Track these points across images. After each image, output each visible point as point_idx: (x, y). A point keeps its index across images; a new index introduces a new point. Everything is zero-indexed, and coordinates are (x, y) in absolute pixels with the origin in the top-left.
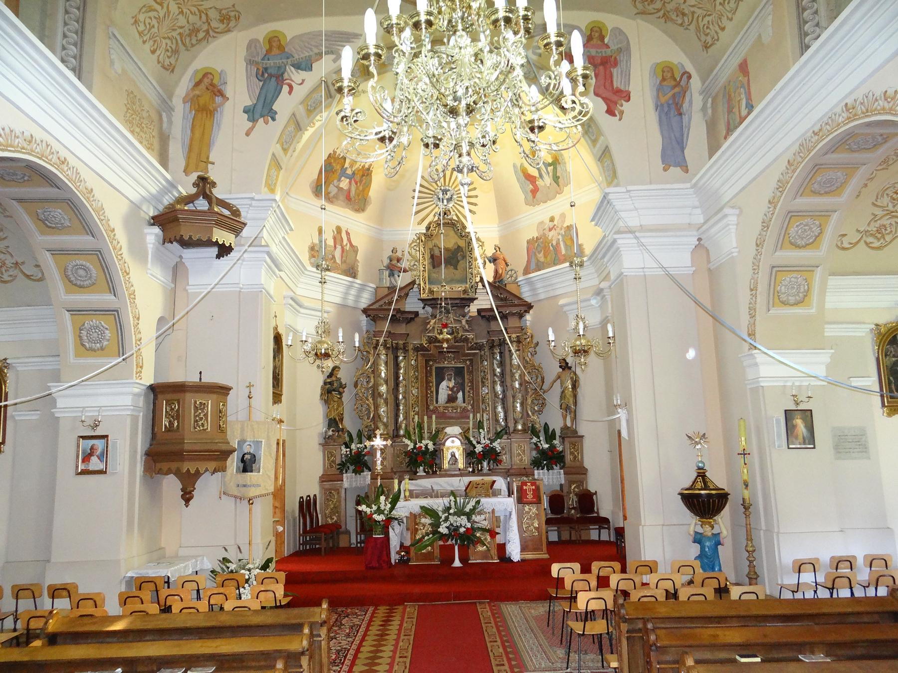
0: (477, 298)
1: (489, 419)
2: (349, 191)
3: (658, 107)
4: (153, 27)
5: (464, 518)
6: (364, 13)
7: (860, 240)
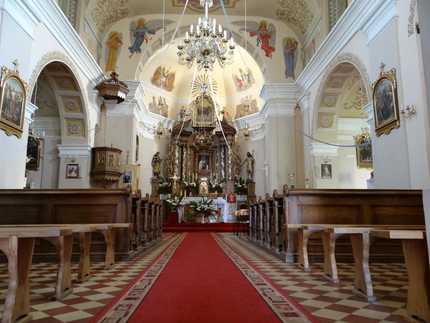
0: (215, 128)
1: (218, 176)
2: (165, 83)
3: (285, 54)
4: (98, 16)
5: (207, 205)
6: (185, 33)
7: (352, 106)
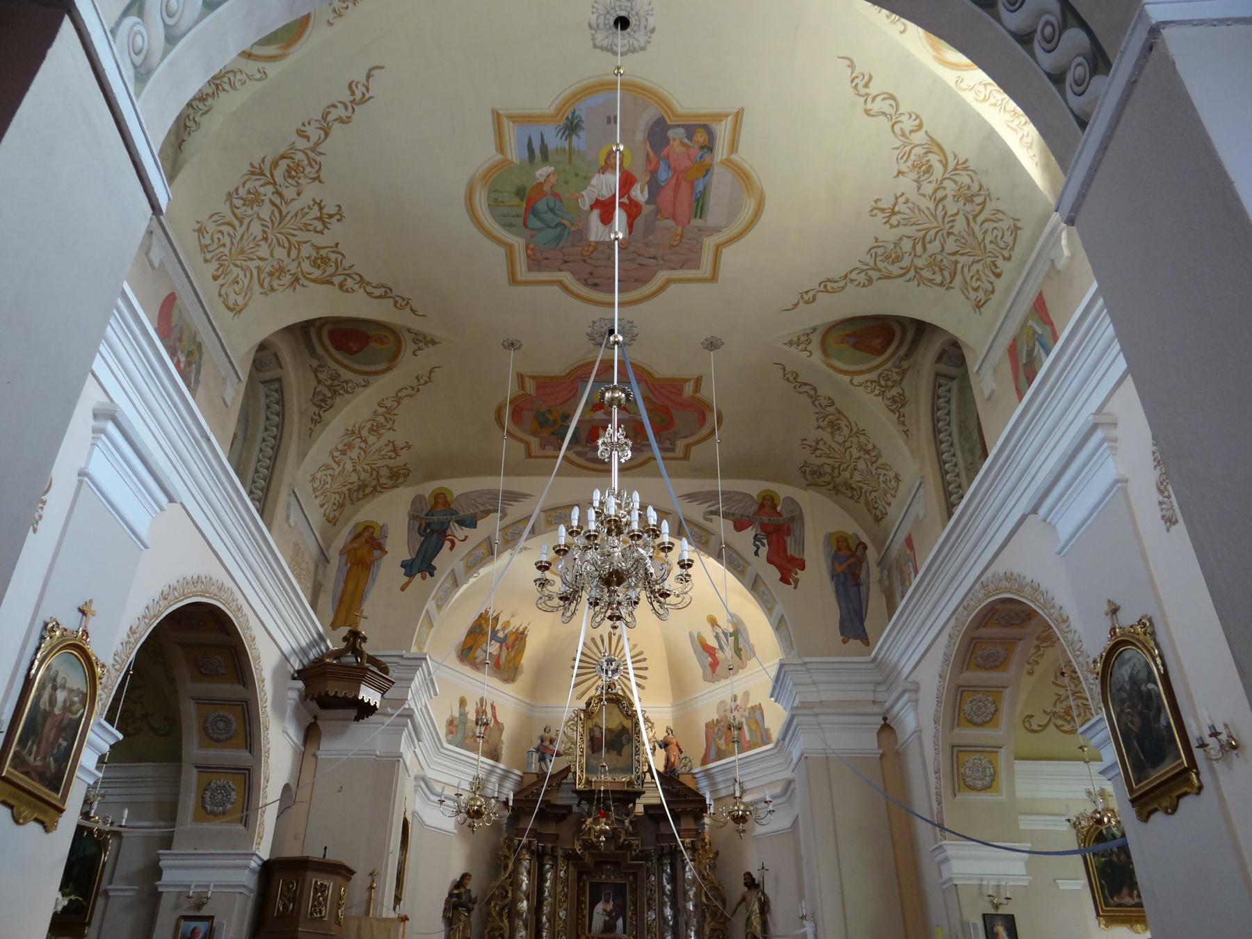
0: (644, 793)
2: (499, 657)
3: (834, 576)
